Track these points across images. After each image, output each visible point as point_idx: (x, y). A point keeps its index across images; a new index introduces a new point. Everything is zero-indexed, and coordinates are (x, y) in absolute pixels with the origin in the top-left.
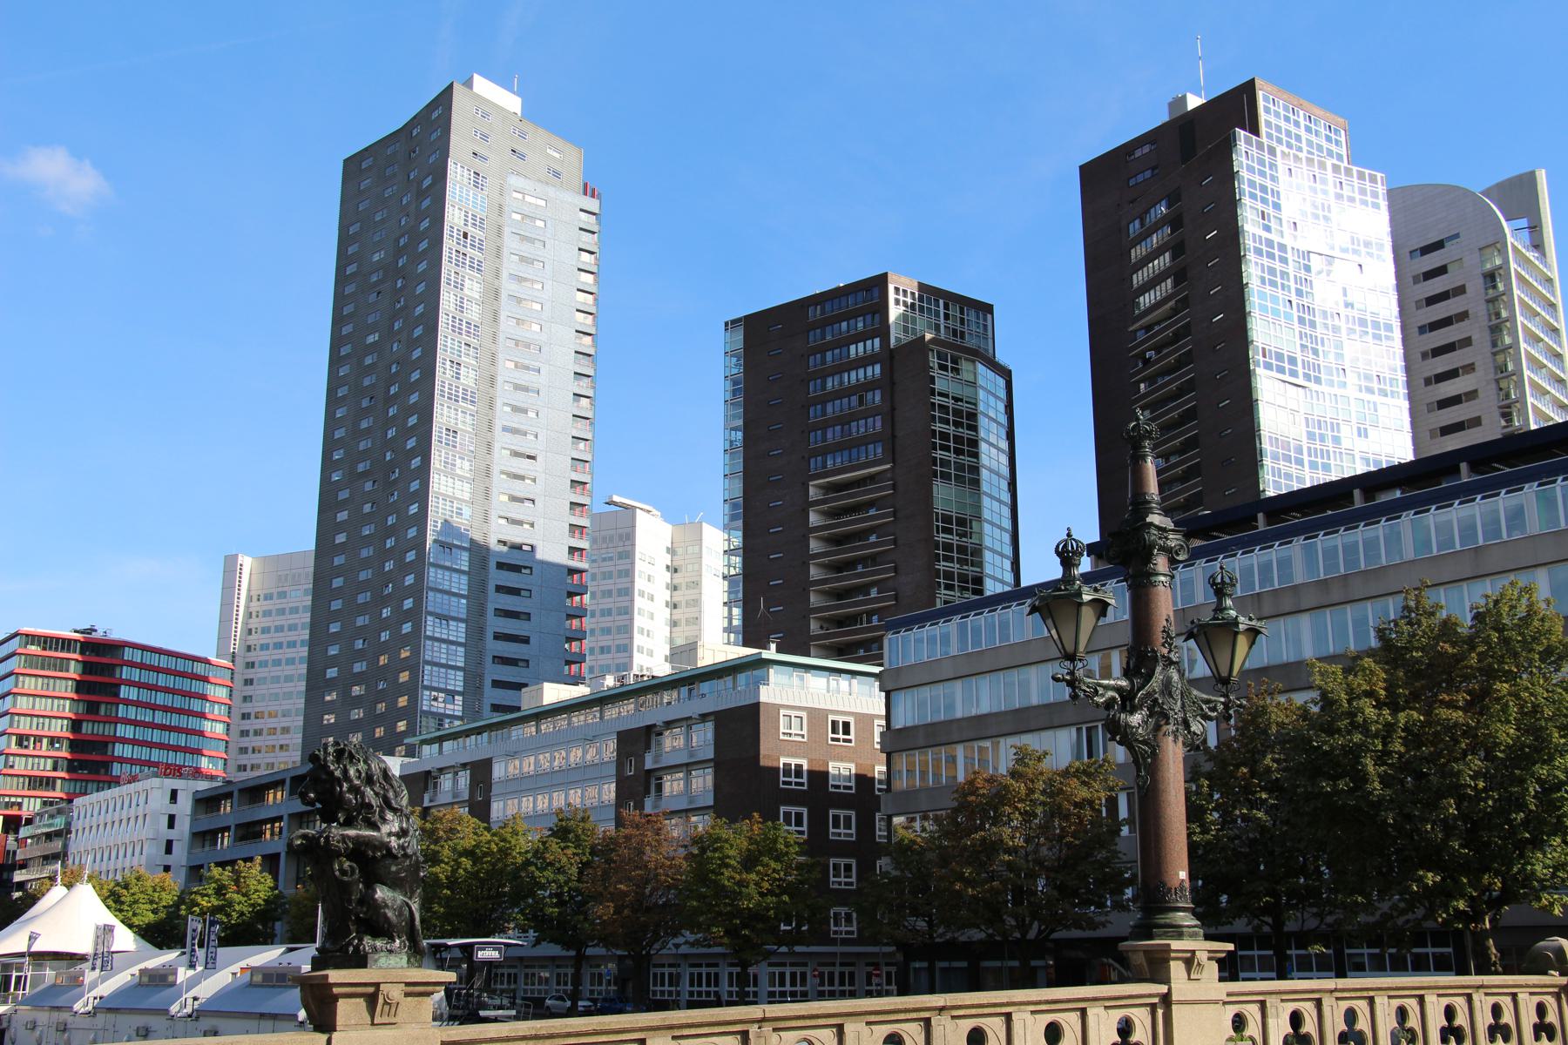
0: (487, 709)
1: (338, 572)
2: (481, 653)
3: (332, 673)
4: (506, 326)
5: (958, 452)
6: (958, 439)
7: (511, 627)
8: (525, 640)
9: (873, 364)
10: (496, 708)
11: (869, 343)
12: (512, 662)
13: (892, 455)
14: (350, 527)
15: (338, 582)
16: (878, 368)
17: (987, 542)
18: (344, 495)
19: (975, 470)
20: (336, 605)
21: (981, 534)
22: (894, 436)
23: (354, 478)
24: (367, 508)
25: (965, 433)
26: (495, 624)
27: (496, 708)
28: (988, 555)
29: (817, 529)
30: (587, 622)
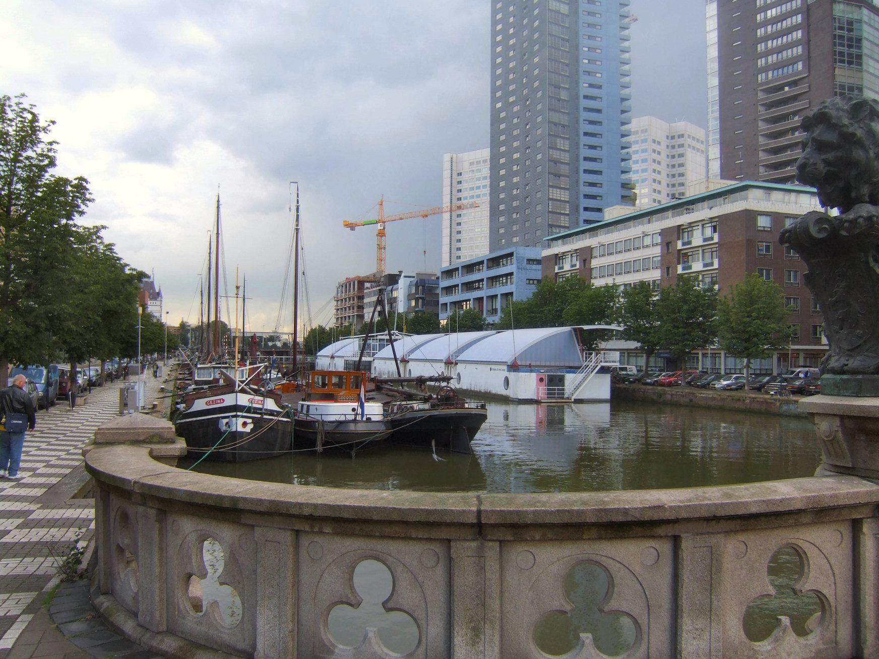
0: (581, 222)
1: (502, 155)
2: (577, 193)
3: (502, 207)
4: (583, 18)
5: (850, 46)
6: (850, 55)
7: (593, 116)
8: (600, 123)
9: (797, 46)
10: (587, 222)
11: (795, 49)
12: (593, 135)
13: (809, 66)
14: (508, 154)
15: (502, 161)
16: (800, 48)
17: (865, 35)
18: (503, 115)
19: (859, 57)
20: (502, 172)
21: (861, 30)
22: (809, 57)
23: (507, 106)
24: (515, 121)
25: (854, 51)
26: (585, 152)
27: (587, 222)
28: (865, 44)
29: (762, 130)
30: (631, 138)
